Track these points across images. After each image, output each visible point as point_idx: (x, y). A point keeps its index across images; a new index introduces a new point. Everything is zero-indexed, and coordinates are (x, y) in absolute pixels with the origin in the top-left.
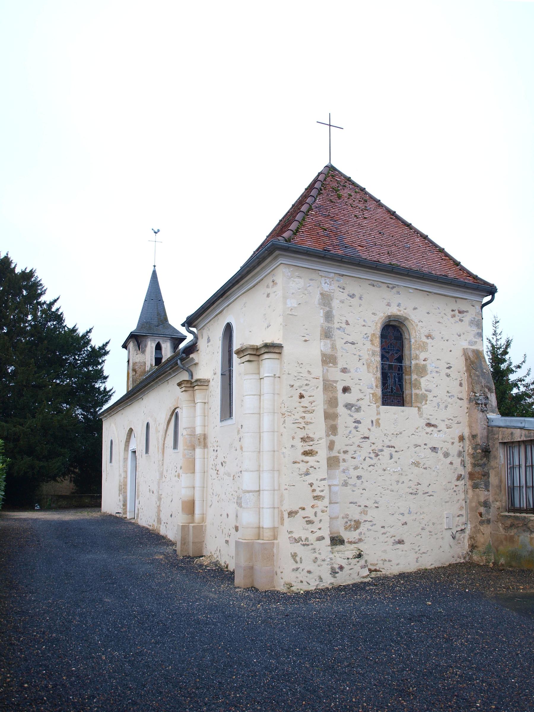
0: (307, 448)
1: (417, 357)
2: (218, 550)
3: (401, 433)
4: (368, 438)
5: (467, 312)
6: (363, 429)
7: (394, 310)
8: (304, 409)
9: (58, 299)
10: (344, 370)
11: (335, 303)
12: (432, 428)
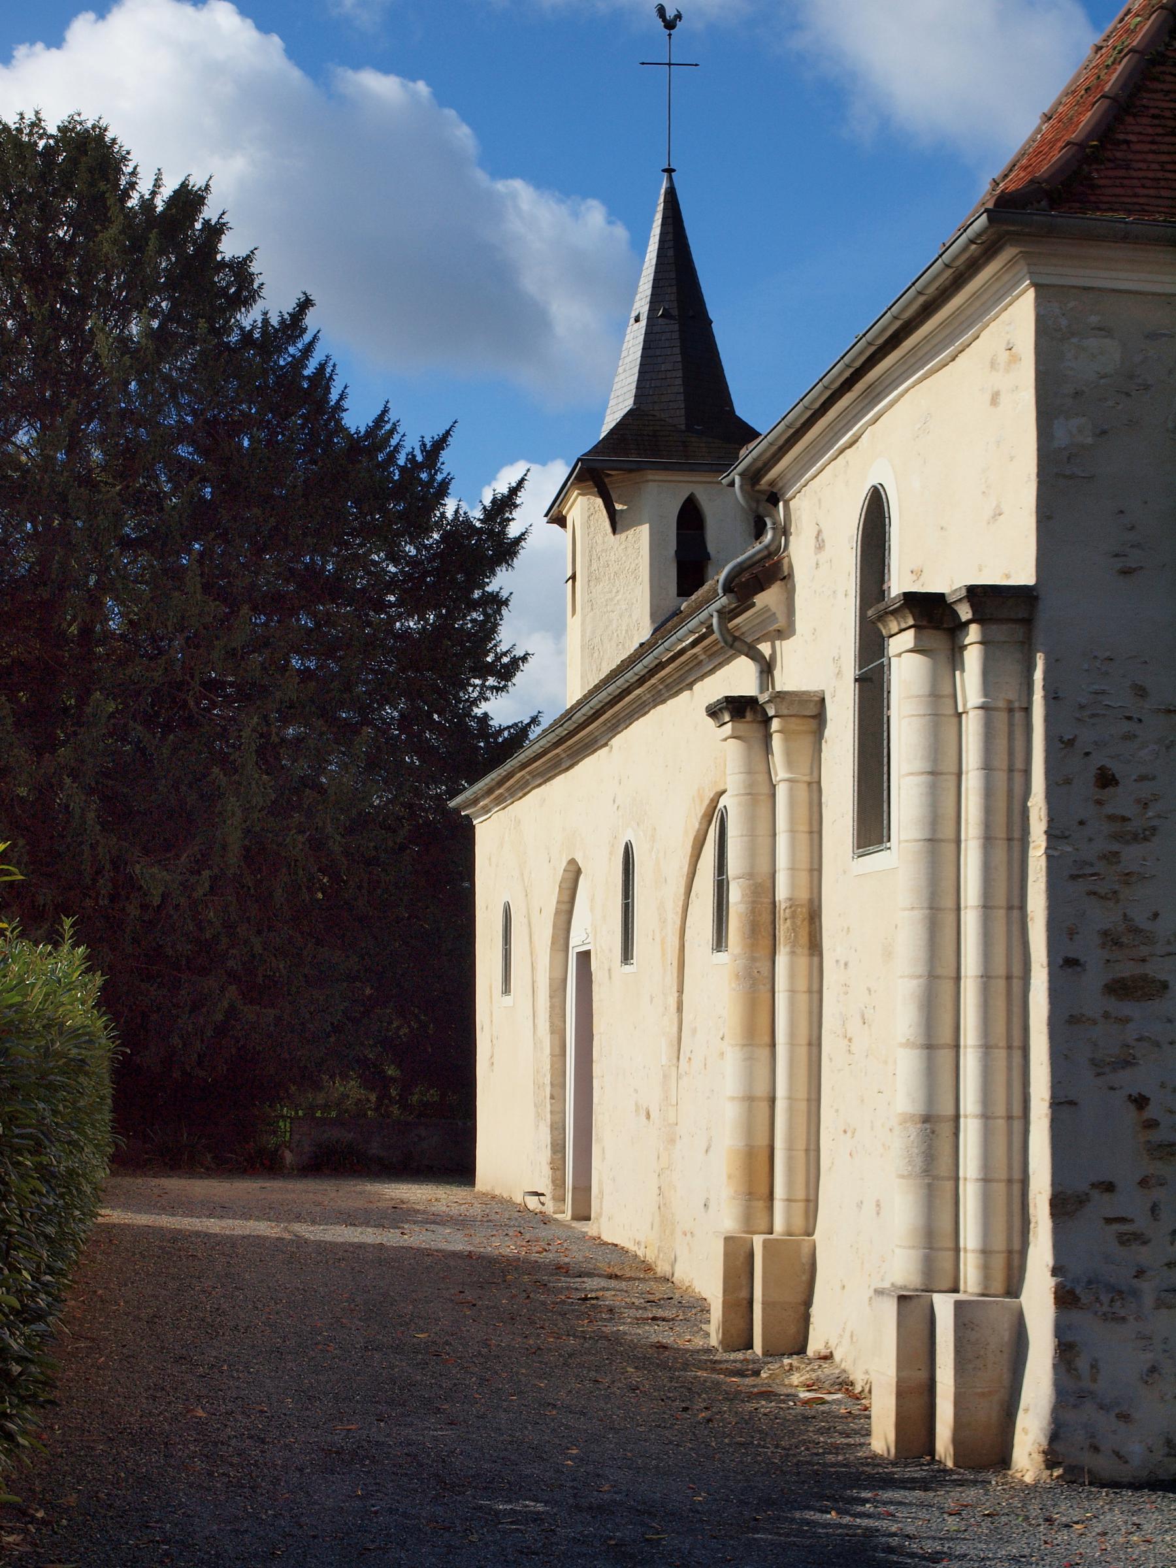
0: (1127, 970)
2: (847, 1335)
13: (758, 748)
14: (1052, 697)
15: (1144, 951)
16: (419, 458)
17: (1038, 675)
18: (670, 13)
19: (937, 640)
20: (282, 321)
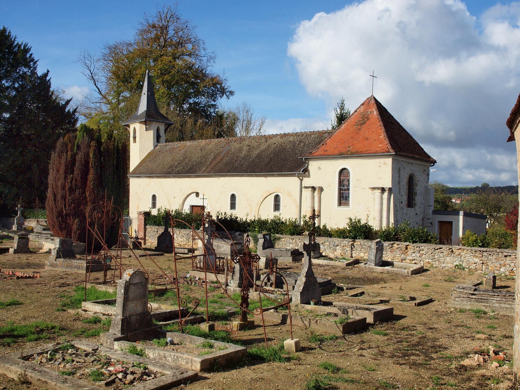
9: (71, 99)
17: (392, 196)
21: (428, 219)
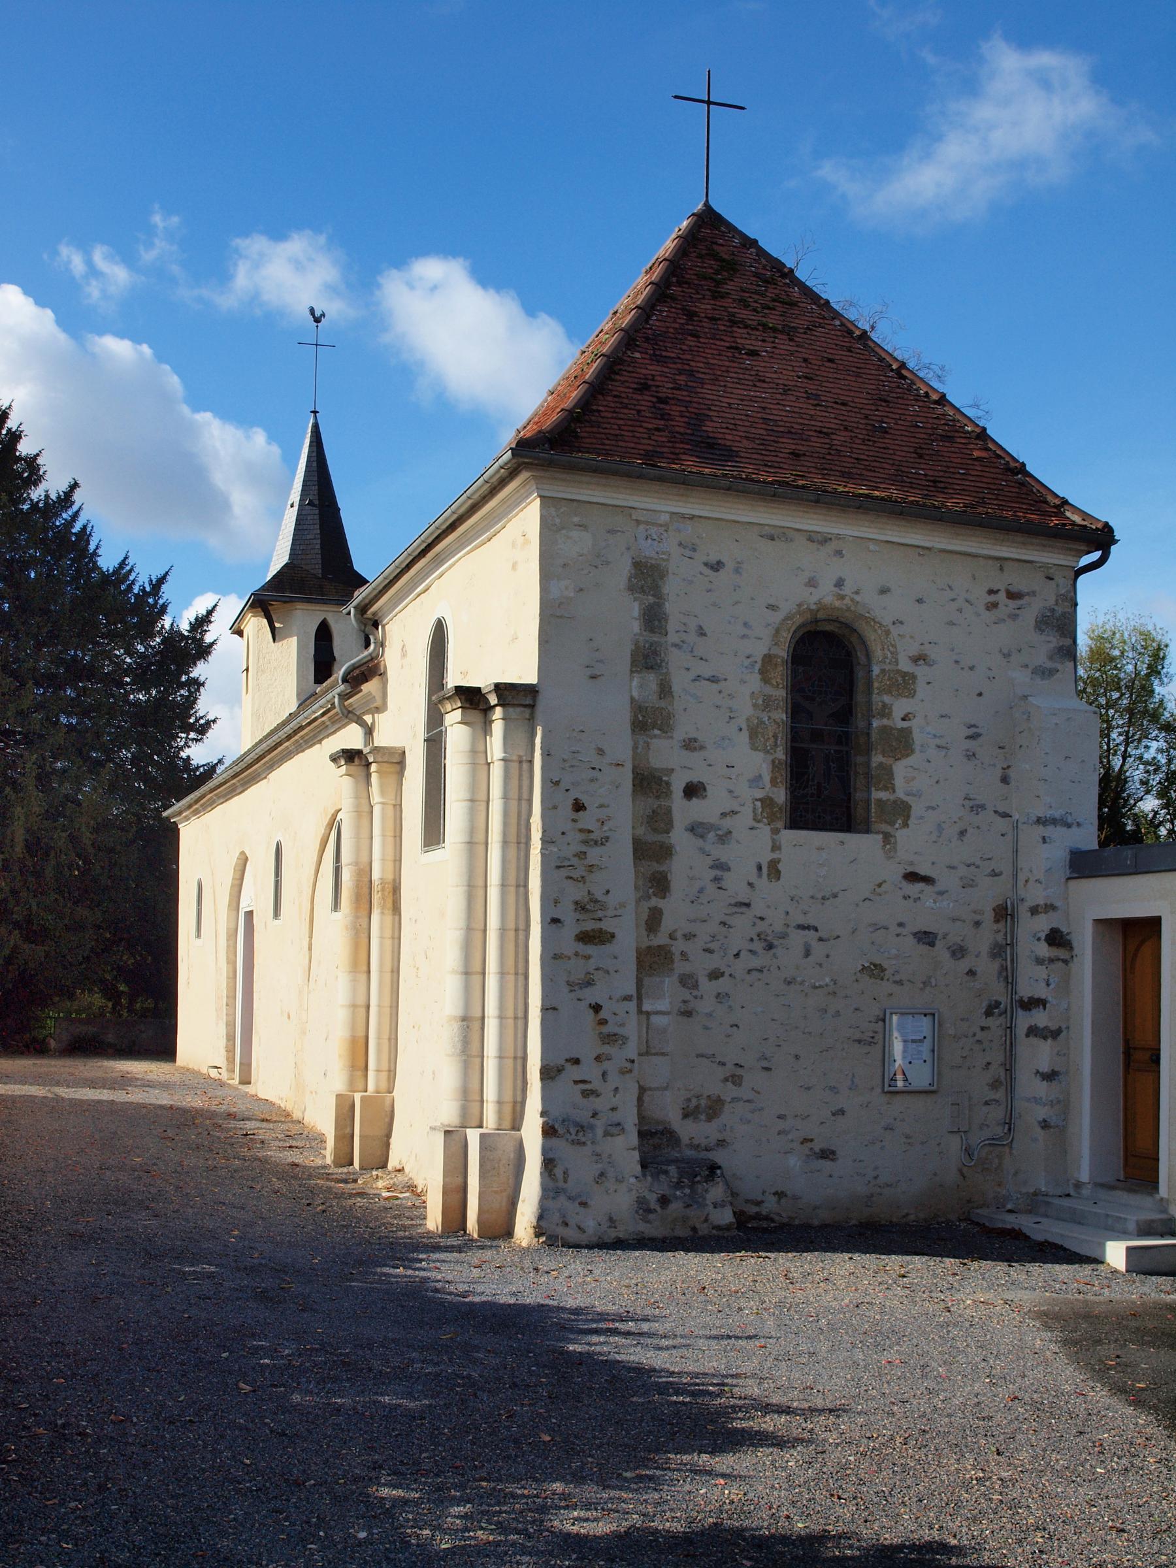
0: (589, 926)
1: (886, 712)
3: (835, 896)
4: (748, 905)
5: (1034, 593)
6: (736, 885)
7: (825, 594)
8: (583, 836)
10: (690, 745)
11: (671, 587)
12: (920, 886)
13: (363, 784)
14: (546, 754)
15: (600, 914)
16: (148, 589)
18: (318, 314)
19: (475, 716)
20: (59, 497)
21: (1034, 911)
